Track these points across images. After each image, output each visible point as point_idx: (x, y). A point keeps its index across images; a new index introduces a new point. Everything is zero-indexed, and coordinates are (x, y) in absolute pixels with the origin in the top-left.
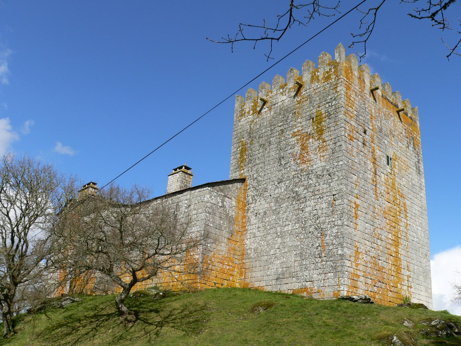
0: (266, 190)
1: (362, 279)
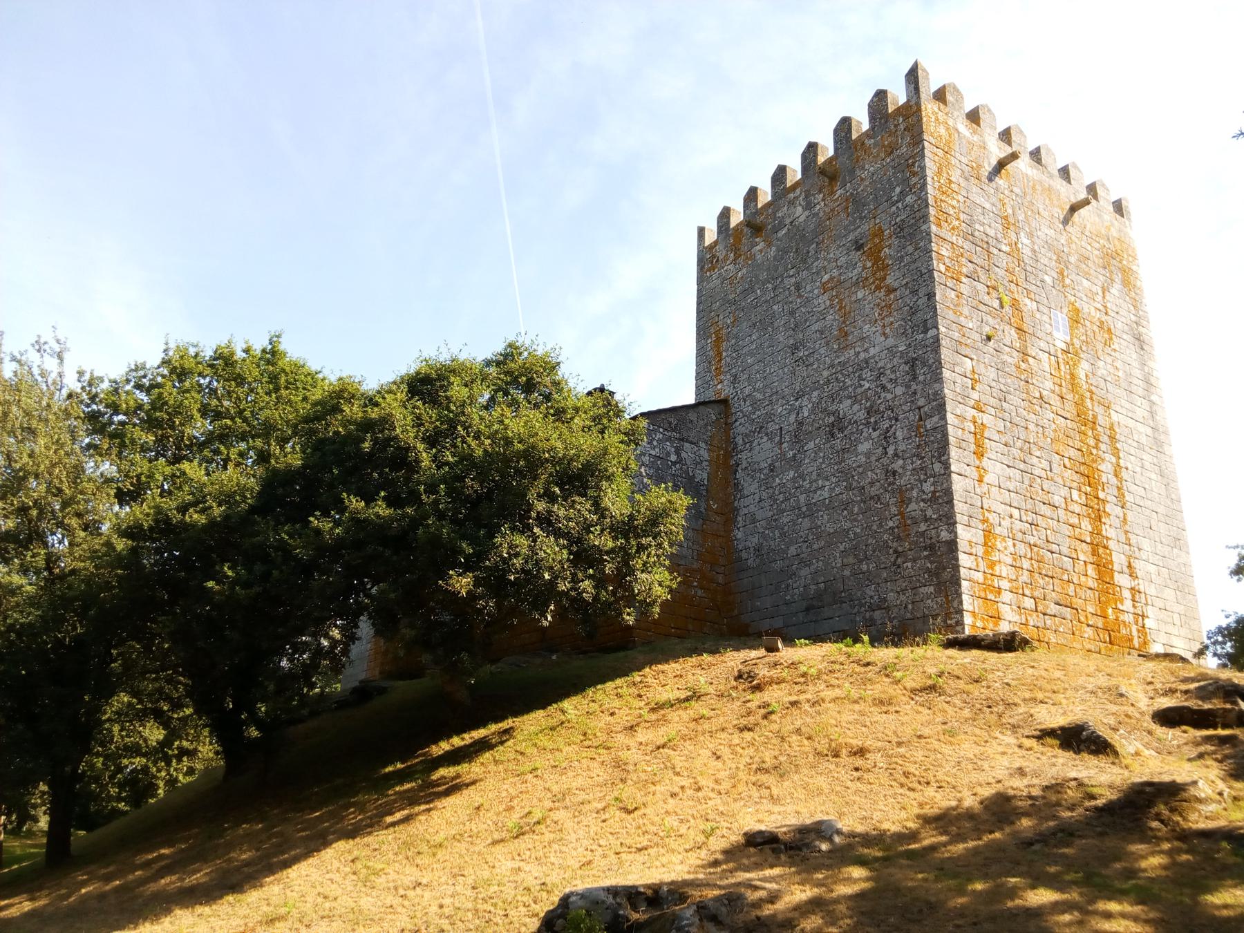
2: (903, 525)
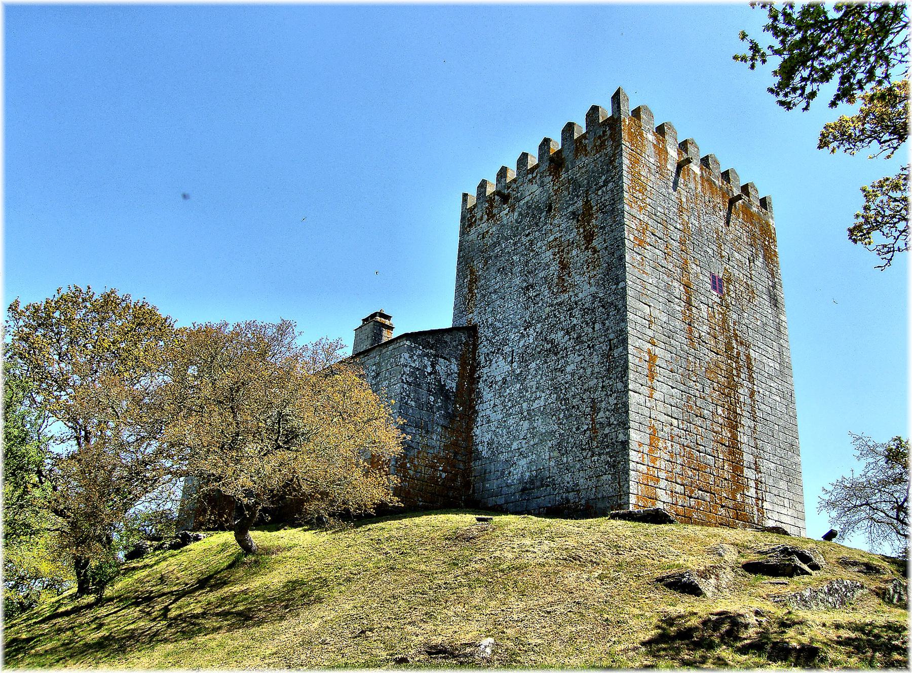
0: (505, 342)
1: (663, 484)
2: (594, 430)
